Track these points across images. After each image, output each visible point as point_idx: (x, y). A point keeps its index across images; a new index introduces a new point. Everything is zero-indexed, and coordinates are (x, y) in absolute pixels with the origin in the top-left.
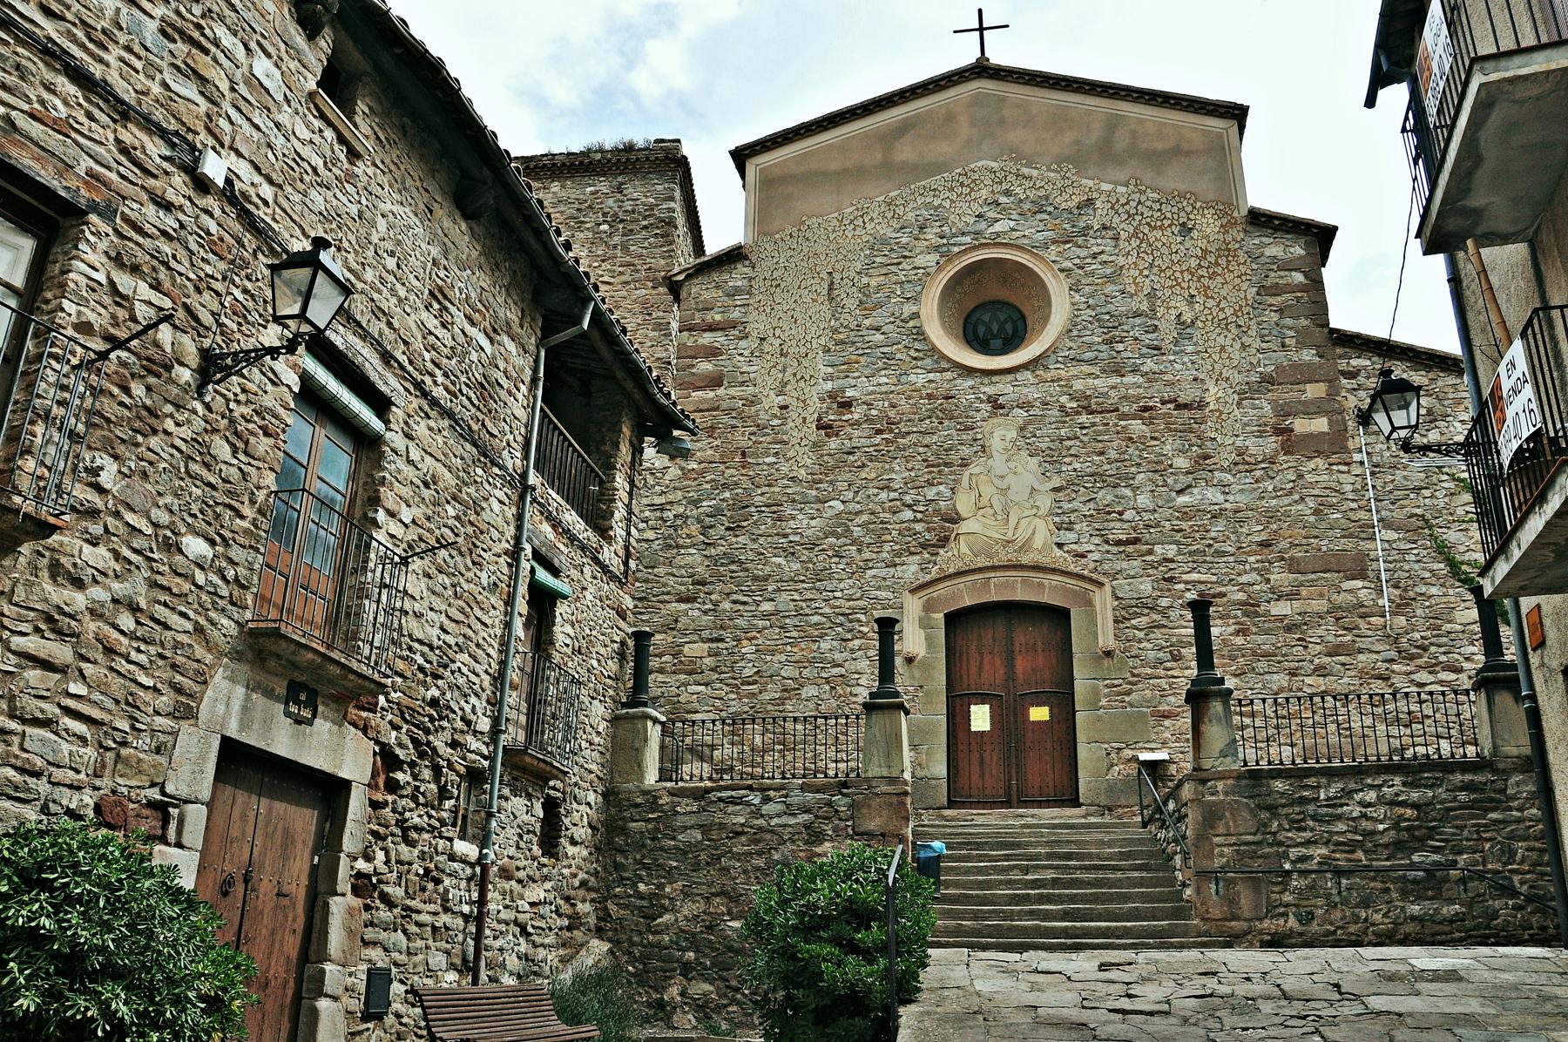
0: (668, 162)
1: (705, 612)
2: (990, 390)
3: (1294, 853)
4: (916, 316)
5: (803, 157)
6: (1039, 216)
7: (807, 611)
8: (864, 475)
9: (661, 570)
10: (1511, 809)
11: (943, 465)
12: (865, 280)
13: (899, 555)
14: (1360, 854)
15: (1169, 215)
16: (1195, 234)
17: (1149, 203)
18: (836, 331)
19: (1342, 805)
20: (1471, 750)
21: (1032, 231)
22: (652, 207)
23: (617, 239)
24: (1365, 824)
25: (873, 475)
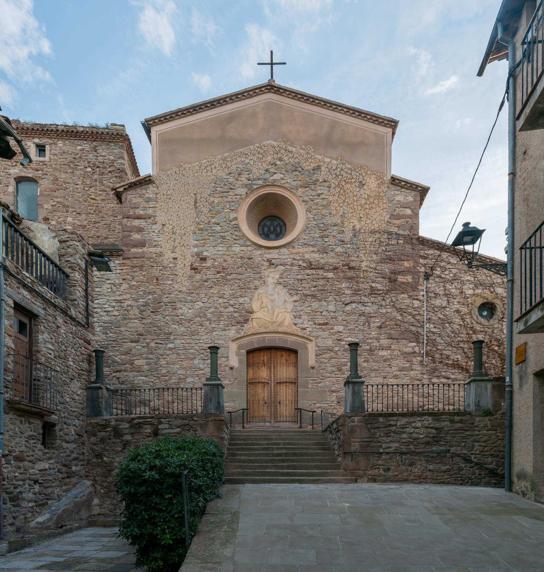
0: (116, 137)
1: (144, 347)
2: (269, 256)
3: (384, 446)
4: (236, 219)
5: (181, 129)
6: (295, 173)
7: (188, 348)
8: (212, 291)
9: (123, 329)
10: (475, 430)
11: (246, 288)
12: (212, 199)
13: (227, 326)
14: (412, 447)
15: (355, 177)
16: (365, 187)
17: (346, 170)
18: (198, 224)
19: (406, 428)
20: (451, 407)
21: (290, 180)
22: (113, 161)
23: (96, 177)
24: (414, 435)
25: (216, 292)
